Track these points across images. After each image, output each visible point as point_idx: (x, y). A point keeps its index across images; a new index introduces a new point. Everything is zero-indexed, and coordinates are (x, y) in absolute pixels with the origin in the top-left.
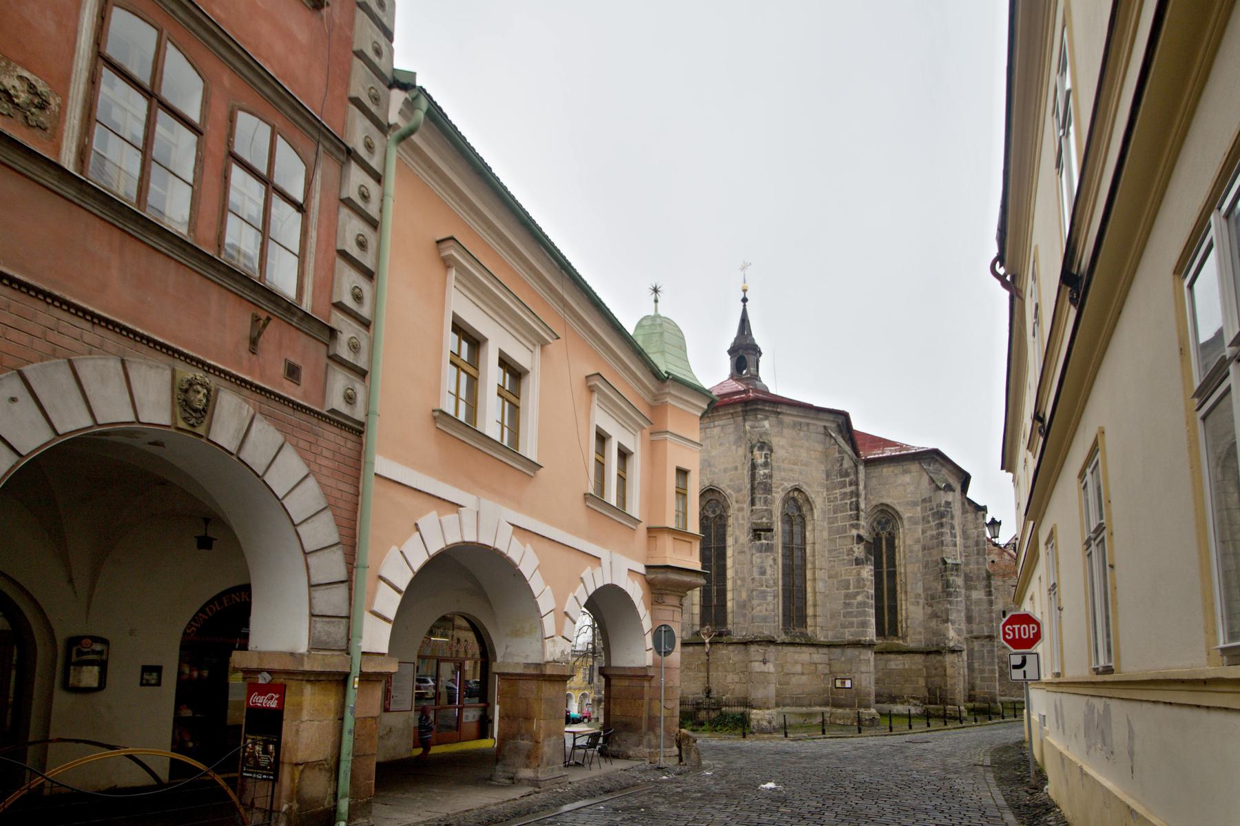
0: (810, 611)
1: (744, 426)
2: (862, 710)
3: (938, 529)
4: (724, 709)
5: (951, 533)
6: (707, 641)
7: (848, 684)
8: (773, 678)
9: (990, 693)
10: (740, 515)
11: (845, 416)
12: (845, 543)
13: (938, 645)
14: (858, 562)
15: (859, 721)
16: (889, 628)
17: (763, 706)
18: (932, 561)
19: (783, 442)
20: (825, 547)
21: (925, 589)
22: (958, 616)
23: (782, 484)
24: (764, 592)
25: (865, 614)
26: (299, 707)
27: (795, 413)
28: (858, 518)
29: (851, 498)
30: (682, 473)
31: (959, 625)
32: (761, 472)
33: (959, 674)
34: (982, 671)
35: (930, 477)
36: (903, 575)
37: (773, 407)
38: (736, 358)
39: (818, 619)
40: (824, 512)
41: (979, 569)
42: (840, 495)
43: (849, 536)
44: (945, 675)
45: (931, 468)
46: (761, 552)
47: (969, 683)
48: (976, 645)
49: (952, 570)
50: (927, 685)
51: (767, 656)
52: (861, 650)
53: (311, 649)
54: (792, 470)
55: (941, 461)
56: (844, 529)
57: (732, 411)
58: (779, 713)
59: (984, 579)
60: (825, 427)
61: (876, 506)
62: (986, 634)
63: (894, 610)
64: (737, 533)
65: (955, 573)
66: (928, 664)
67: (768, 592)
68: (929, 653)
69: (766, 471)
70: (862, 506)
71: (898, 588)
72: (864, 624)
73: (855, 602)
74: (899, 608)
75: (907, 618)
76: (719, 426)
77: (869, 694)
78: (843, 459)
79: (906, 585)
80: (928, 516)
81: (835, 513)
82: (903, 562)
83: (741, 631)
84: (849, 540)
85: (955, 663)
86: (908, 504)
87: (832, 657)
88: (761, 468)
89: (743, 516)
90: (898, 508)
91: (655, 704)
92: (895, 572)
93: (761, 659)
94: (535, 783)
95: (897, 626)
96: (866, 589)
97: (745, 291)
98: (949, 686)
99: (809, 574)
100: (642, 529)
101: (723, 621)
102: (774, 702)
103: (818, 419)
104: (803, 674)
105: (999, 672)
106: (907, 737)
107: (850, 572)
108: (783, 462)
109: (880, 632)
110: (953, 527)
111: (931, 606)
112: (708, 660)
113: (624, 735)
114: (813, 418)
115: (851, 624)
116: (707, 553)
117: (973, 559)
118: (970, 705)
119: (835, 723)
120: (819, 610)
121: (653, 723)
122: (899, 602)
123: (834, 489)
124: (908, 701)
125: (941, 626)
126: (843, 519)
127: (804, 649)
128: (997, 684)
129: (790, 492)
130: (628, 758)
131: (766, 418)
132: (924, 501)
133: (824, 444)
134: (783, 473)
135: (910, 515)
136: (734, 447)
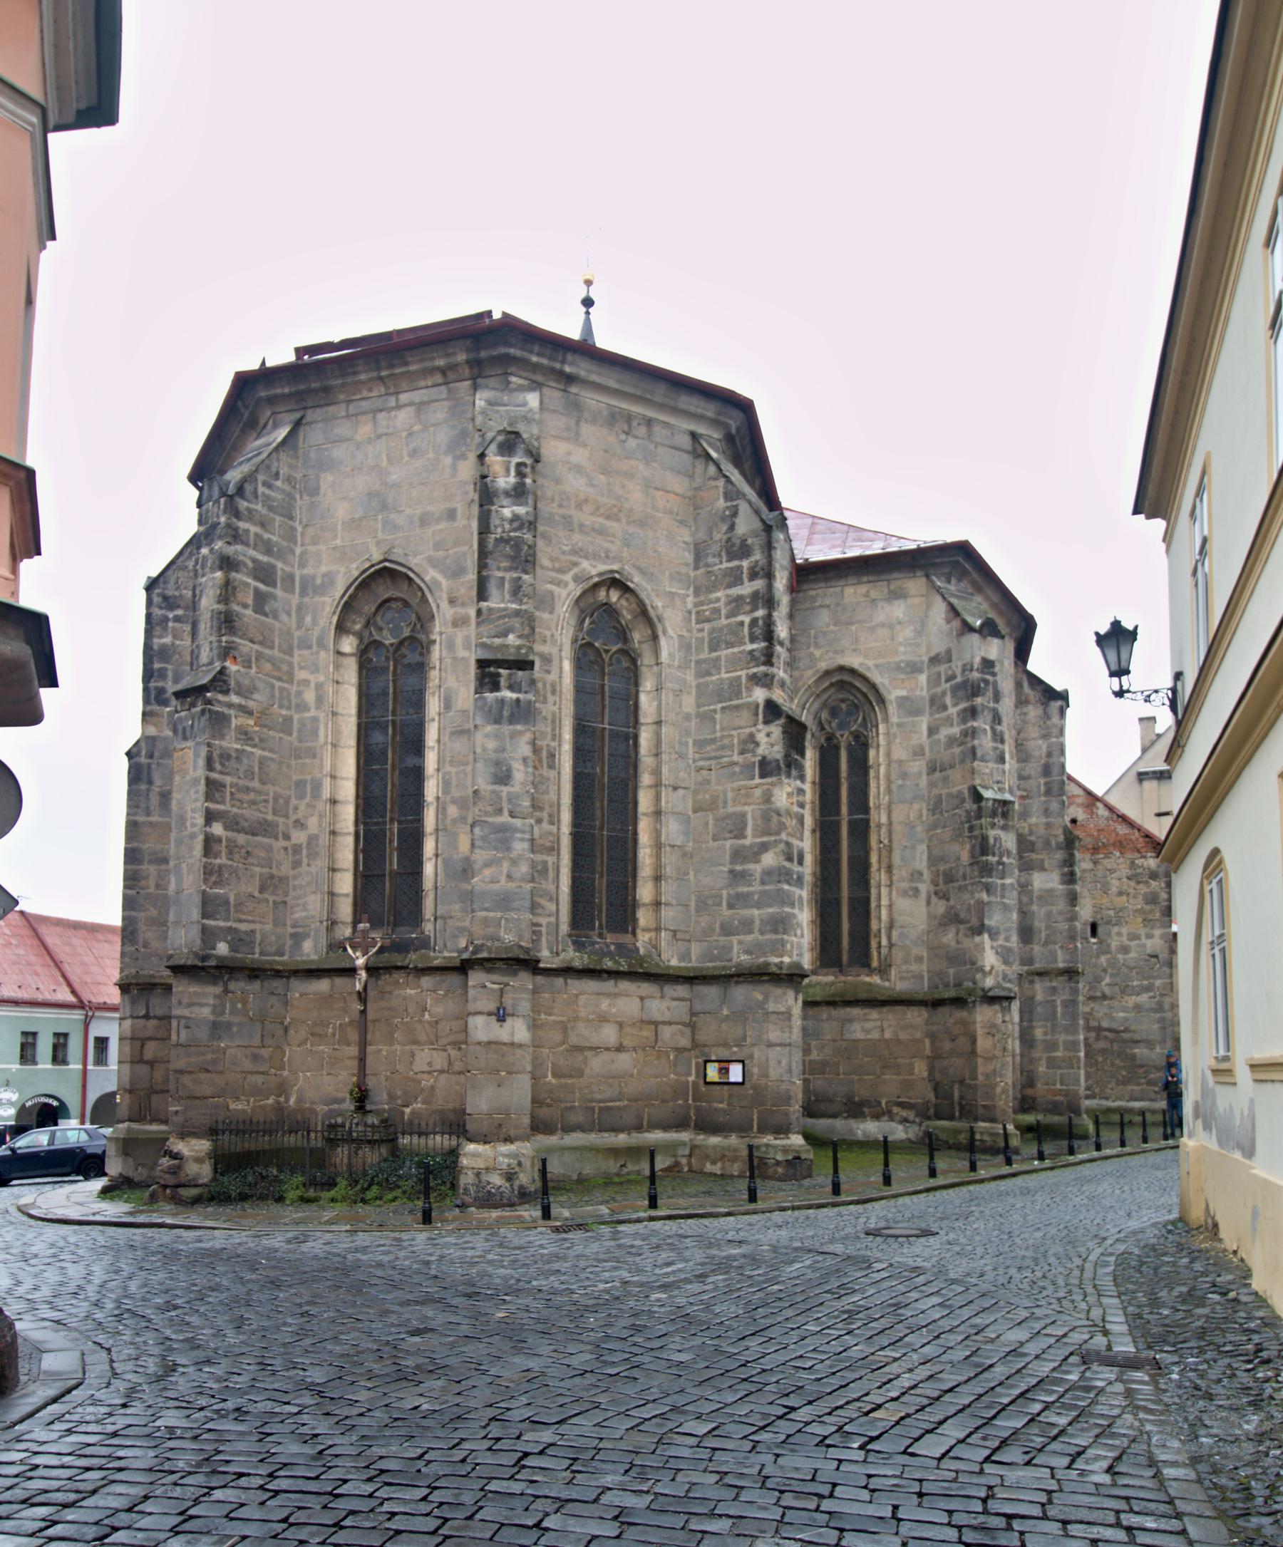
0: (645, 892)
3: (964, 721)
4: (405, 1141)
5: (994, 731)
6: (361, 962)
7: (736, 1073)
8: (525, 1060)
9: (1067, 1093)
11: (745, 407)
12: (738, 722)
13: (958, 985)
18: (949, 795)
19: (580, 456)
20: (688, 734)
21: (933, 861)
22: (1002, 919)
23: (576, 564)
24: (503, 829)
27: (613, 384)
28: (768, 658)
29: (755, 609)
31: (1007, 939)
33: (1005, 1049)
34: (1052, 1046)
36: (884, 830)
37: (551, 358)
39: (667, 914)
40: (686, 646)
41: (1048, 826)
42: (727, 604)
45: (952, 587)
46: (498, 721)
47: (1022, 1072)
48: (1040, 990)
49: (994, 814)
50: (931, 1077)
51: (508, 1001)
54: (602, 532)
55: (975, 575)
56: (735, 689)
57: (441, 362)
59: (1059, 847)
60: (694, 436)
61: (827, 673)
62: (1061, 965)
63: (862, 908)
64: (451, 682)
65: (999, 821)
66: (935, 1028)
67: (516, 830)
68: (937, 1004)
69: (521, 510)
71: (874, 859)
72: (781, 925)
73: (756, 869)
74: (873, 904)
75: (891, 926)
76: (411, 404)
77: (787, 1099)
78: (735, 514)
79: (890, 851)
80: (944, 693)
81: (713, 648)
82: (885, 800)
83: (455, 937)
84: (746, 716)
85: (994, 1026)
86: (898, 668)
87: (698, 1007)
88: (505, 502)
89: (467, 638)
90: (877, 678)
92: (867, 821)
93: (492, 1006)
95: (868, 944)
96: (784, 836)
97: (588, 283)
98: (981, 1078)
99: (645, 801)
101: (416, 917)
102: (526, 1121)
104: (620, 1048)
106: (876, 1214)
107: (748, 795)
108: (579, 506)
110: (997, 719)
111: (945, 897)
112: (363, 1012)
114: (662, 407)
115: (747, 926)
116: (377, 737)
117: (1036, 804)
119: (702, 1173)
122: (873, 891)
123: (714, 587)
124: (890, 1112)
125: (968, 943)
126: (733, 663)
127: (625, 985)
128: (1082, 1072)
129: (596, 586)
131: (536, 386)
132: (935, 660)
133: (692, 477)
134: (577, 538)
135: (904, 693)
136: (448, 460)
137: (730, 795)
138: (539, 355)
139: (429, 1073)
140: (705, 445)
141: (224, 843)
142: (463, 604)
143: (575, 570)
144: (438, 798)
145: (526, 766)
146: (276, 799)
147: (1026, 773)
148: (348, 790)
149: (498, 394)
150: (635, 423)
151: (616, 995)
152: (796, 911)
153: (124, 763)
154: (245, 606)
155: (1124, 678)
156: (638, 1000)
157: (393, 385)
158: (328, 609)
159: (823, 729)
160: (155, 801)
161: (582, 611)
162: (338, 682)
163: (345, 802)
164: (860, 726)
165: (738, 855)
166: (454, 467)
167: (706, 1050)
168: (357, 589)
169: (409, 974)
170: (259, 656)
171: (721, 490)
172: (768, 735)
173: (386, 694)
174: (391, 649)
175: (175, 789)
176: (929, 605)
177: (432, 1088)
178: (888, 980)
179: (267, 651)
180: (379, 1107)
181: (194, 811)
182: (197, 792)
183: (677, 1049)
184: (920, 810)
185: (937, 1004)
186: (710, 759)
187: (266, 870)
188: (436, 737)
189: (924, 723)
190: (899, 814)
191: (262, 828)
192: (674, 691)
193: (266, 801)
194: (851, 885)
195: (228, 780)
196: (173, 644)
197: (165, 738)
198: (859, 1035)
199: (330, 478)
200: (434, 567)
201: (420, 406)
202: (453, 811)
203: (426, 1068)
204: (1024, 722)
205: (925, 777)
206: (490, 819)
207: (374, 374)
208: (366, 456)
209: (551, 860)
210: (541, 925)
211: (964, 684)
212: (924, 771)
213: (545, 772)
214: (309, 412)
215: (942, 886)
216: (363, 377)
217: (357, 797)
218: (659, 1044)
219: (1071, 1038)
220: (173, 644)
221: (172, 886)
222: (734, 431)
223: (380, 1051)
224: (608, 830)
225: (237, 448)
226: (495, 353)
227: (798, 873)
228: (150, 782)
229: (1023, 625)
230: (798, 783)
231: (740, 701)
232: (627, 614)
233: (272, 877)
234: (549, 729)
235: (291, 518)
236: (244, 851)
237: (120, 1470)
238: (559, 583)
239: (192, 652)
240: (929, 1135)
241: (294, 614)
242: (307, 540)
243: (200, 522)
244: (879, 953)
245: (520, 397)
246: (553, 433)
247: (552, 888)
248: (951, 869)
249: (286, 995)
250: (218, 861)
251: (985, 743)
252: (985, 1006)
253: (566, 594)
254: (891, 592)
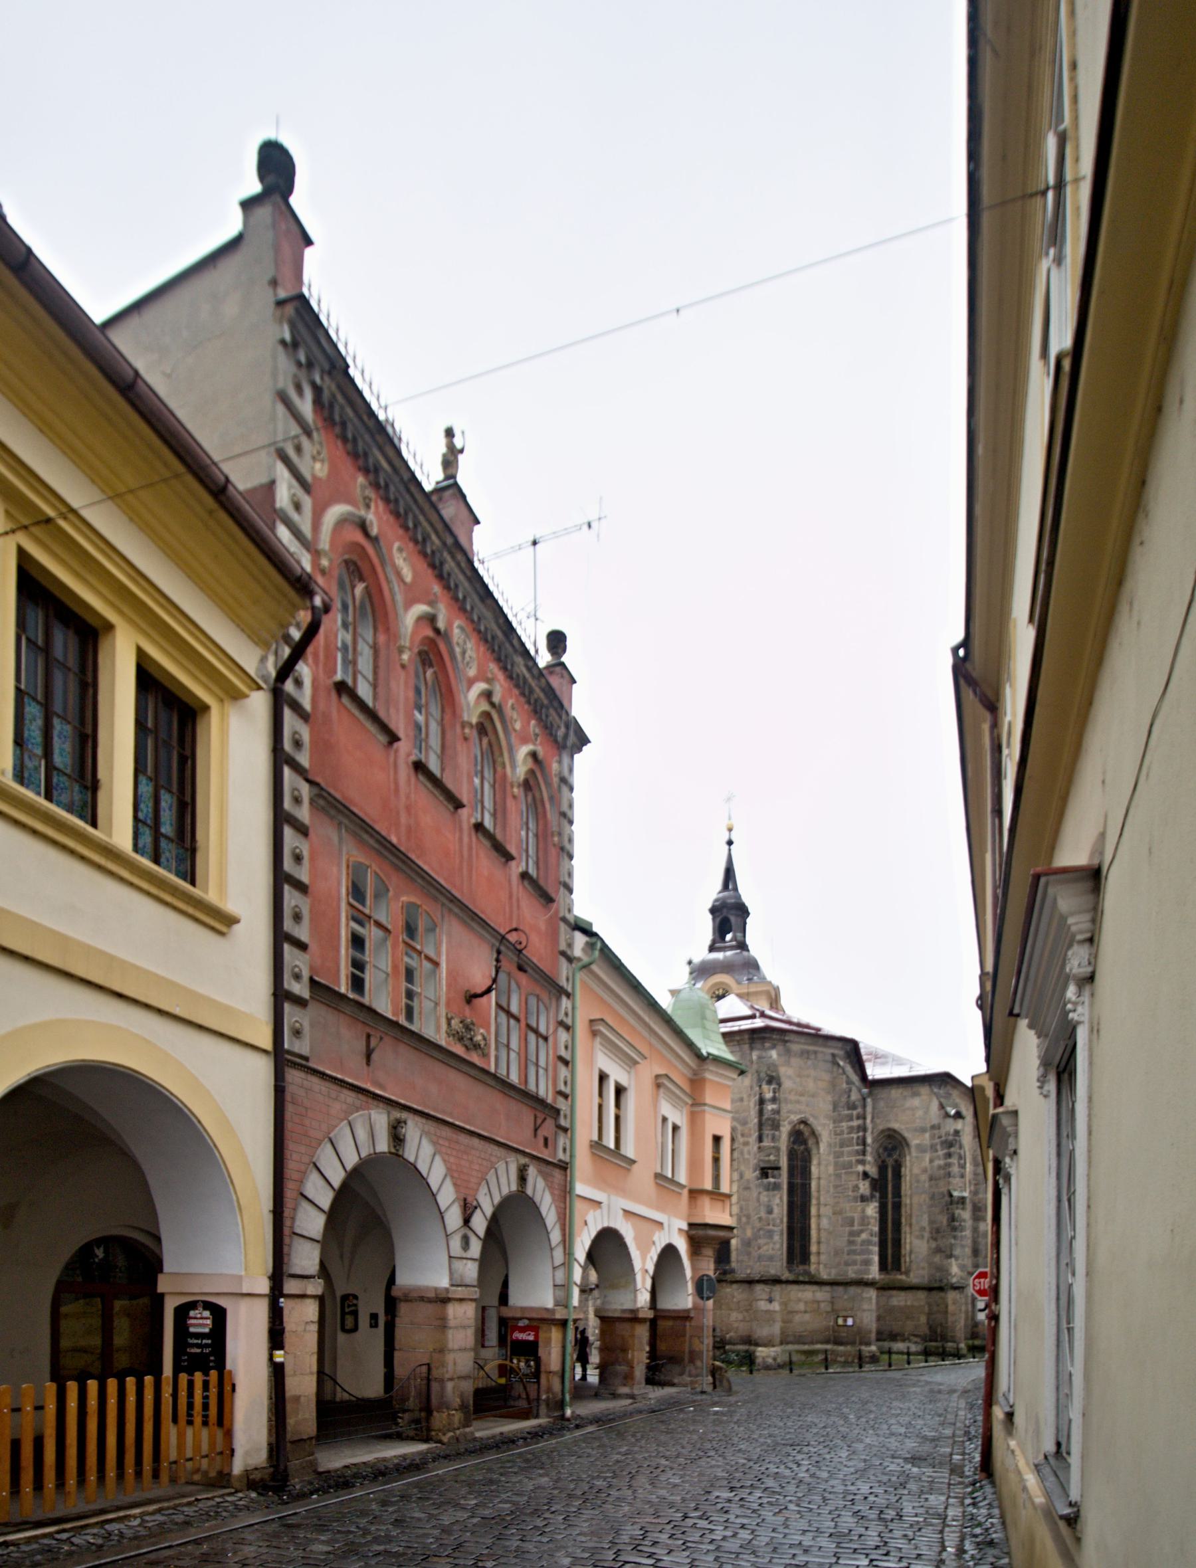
0: (814, 1248)
1: (751, 1054)
2: (863, 1348)
4: (727, 1347)
5: (959, 1164)
7: (850, 1322)
8: (778, 1317)
10: (746, 1149)
13: (941, 1281)
14: (863, 1199)
15: (860, 1358)
16: (893, 1262)
17: (768, 1344)
21: (931, 1222)
25: (870, 1252)
26: (549, 1341)
28: (864, 1153)
30: (717, 1139)
32: (770, 1107)
33: (960, 1310)
36: (908, 1207)
38: (718, 920)
39: (823, 1257)
40: (830, 1145)
49: (958, 1203)
50: (928, 1323)
51: (773, 1295)
52: (862, 1288)
53: (556, 1305)
56: (850, 1165)
58: (783, 1351)
60: (833, 1055)
63: (897, 1243)
65: (960, 1206)
69: (774, 1106)
70: (869, 1140)
71: (903, 1220)
72: (867, 1263)
73: (859, 1240)
74: (903, 1241)
75: (911, 1252)
77: (870, 1332)
78: (850, 1090)
82: (909, 1193)
84: (854, 1177)
86: (916, 1130)
87: (835, 1295)
90: (906, 1134)
91: (696, 1341)
94: (632, 1397)
97: (730, 830)
99: (813, 1211)
100: (685, 1192)
104: (806, 1312)
108: (790, 1093)
109: (883, 1267)
111: (935, 1239)
113: (669, 1367)
118: (970, 1342)
120: (823, 1248)
121: (694, 1356)
122: (903, 1236)
123: (841, 1121)
126: (850, 1154)
127: (807, 1287)
130: (673, 1385)
131: (774, 1047)
132: (933, 1127)
133: (832, 1072)
165: (852, 1234)
176: (930, 1101)
185: (930, 1289)
189: (927, 1157)
190: (915, 1200)
194: (892, 1233)
211: (946, 1141)
212: (927, 1180)
215: (934, 1235)
232: (807, 1134)
240: (926, 1348)
251: (955, 1169)
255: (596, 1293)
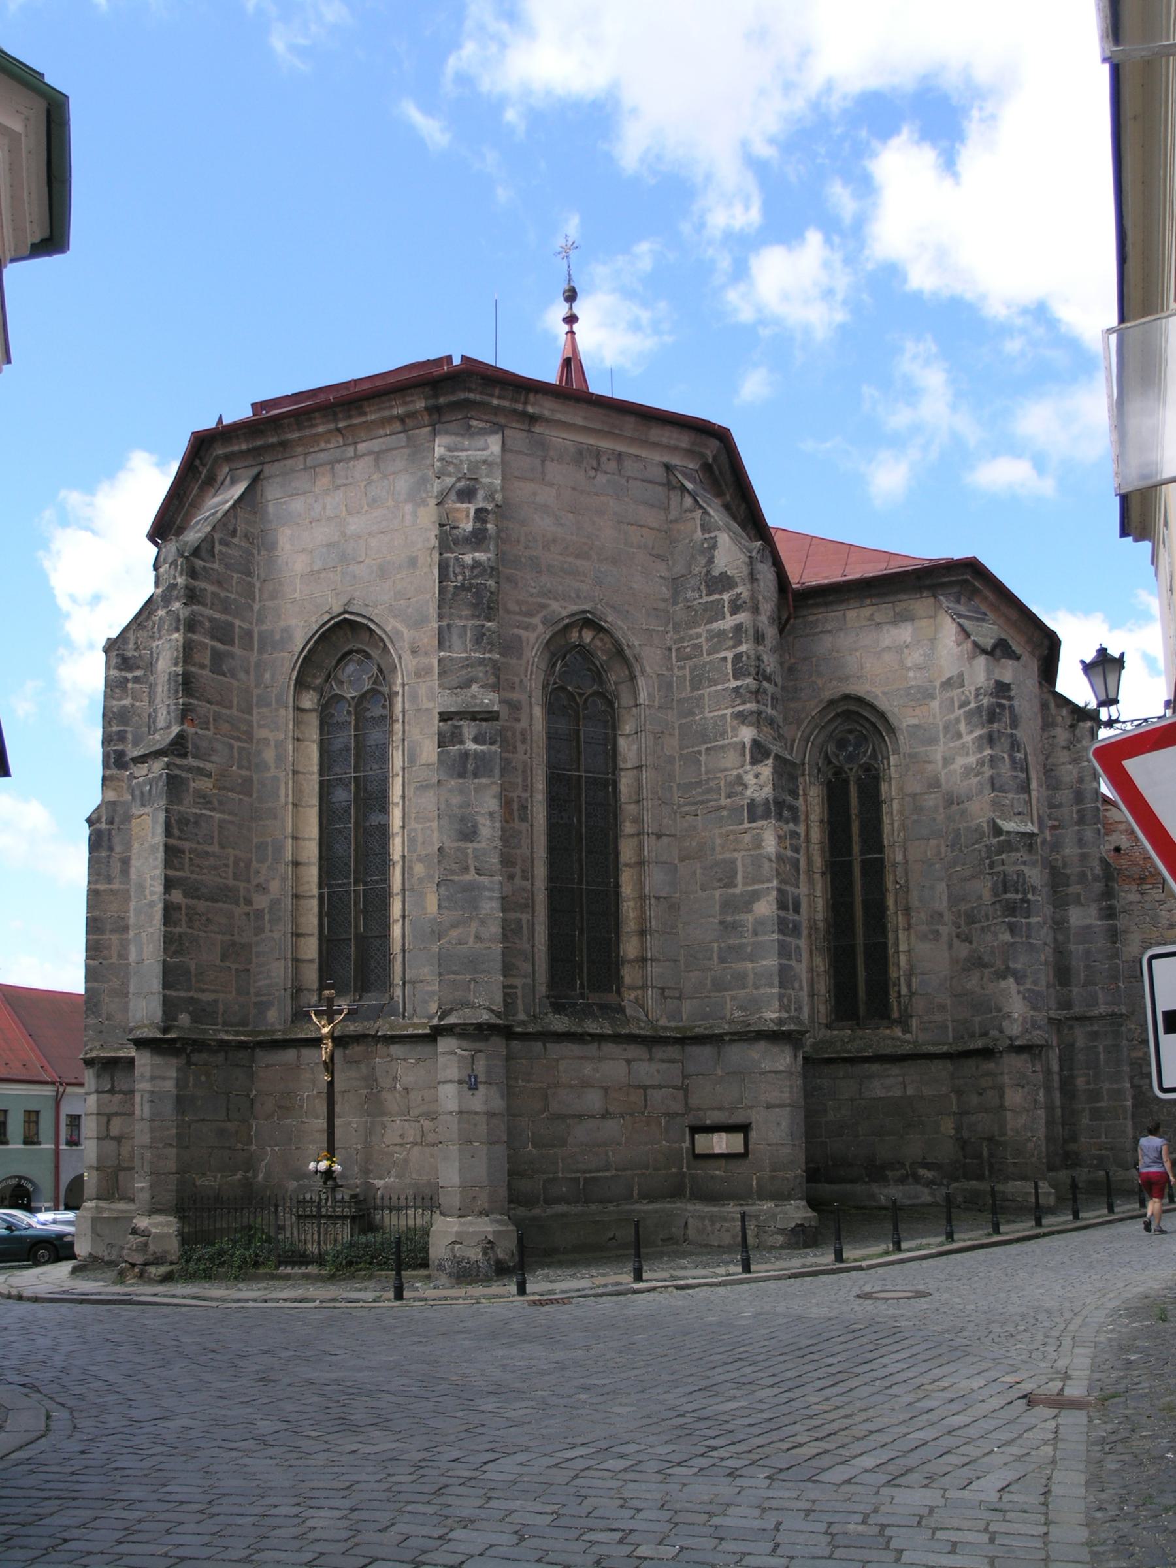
0: (630, 948)
5: (1013, 760)
15: (1074, 1186)
19: (546, 495)
21: (955, 900)
24: (469, 888)
27: (579, 421)
29: (740, 643)
35: (960, 625)
36: (900, 870)
41: (1084, 857)
42: (707, 640)
43: (733, 746)
44: (1002, 1107)
46: (462, 775)
55: (988, 593)
57: (400, 411)
61: (832, 703)
63: (879, 956)
69: (481, 556)
71: (890, 902)
74: (891, 951)
75: (910, 974)
76: (370, 453)
78: (714, 547)
80: (957, 720)
92: (882, 860)
95: (886, 993)
98: (1010, 1133)
99: (627, 852)
103: (645, 443)
104: (606, 1115)
105: (1134, 1097)
112: (331, 1084)
114: (633, 441)
122: (891, 935)
123: (694, 623)
127: (609, 1048)
128: (1129, 1123)
131: (499, 428)
132: (948, 684)
135: (915, 721)
137: (718, 841)
138: (499, 397)
139: (401, 1145)
140: (680, 477)
141: (184, 911)
142: (426, 654)
143: (544, 613)
144: (404, 857)
145: (493, 821)
146: (236, 864)
147: (1056, 801)
148: (311, 851)
149: (459, 439)
150: (604, 459)
151: (600, 1059)
152: (793, 963)
153: (85, 831)
154: (203, 667)
155: (1113, 708)
156: (624, 1063)
157: (349, 435)
158: (288, 665)
159: (830, 762)
160: (116, 867)
161: (553, 654)
162: (298, 739)
163: (308, 864)
164: (870, 758)
165: (728, 905)
166: (415, 515)
167: (701, 1113)
168: (316, 642)
169: (378, 1042)
170: (217, 717)
171: (698, 522)
172: (757, 776)
173: (348, 749)
174: (353, 704)
175: (133, 857)
177: (406, 1161)
178: (910, 1032)
179: (227, 712)
180: (351, 1182)
181: (152, 878)
182: (156, 859)
183: (666, 1114)
184: (938, 846)
186: (696, 803)
187: (227, 938)
188: (400, 793)
191: (225, 894)
192: (654, 734)
193: (226, 866)
195: (187, 845)
196: (132, 705)
197: (124, 803)
198: (881, 1093)
199: (288, 532)
200: (395, 617)
201: (378, 456)
202: (419, 869)
203: (399, 1141)
204: (1052, 746)
205: (941, 810)
206: (456, 878)
207: (332, 426)
208: (324, 508)
209: (525, 917)
210: (516, 987)
213: (518, 825)
214: (266, 467)
215: (964, 928)
216: (320, 429)
217: (321, 858)
218: (649, 1109)
219: (1115, 1086)
220: (132, 705)
221: (133, 957)
222: (710, 460)
223: (350, 1123)
224: (587, 883)
225: (196, 505)
226: (453, 398)
227: (794, 921)
228: (111, 849)
229: (1046, 642)
230: (791, 825)
231: (726, 742)
233: (234, 944)
234: (520, 780)
235: (249, 574)
236: (204, 918)
237: (74, 1499)
238: (526, 628)
239: (150, 715)
241: (252, 673)
242: (265, 597)
243: (157, 584)
244: (899, 1003)
245: (480, 442)
246: (516, 474)
247: (527, 946)
248: (973, 908)
249: (251, 1067)
250: (178, 930)
252: (1013, 1055)
253: (534, 637)
254: (896, 614)
255: (119, 1097)
